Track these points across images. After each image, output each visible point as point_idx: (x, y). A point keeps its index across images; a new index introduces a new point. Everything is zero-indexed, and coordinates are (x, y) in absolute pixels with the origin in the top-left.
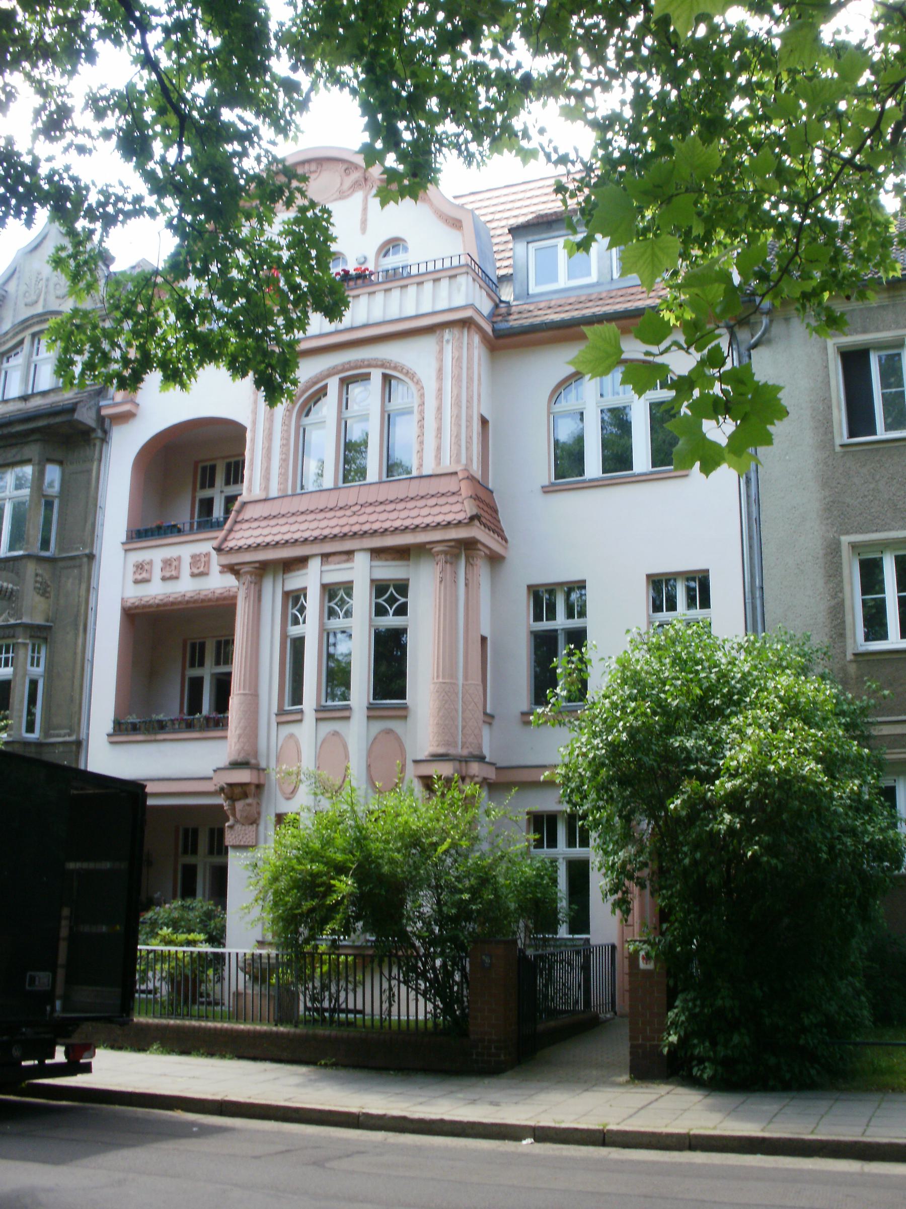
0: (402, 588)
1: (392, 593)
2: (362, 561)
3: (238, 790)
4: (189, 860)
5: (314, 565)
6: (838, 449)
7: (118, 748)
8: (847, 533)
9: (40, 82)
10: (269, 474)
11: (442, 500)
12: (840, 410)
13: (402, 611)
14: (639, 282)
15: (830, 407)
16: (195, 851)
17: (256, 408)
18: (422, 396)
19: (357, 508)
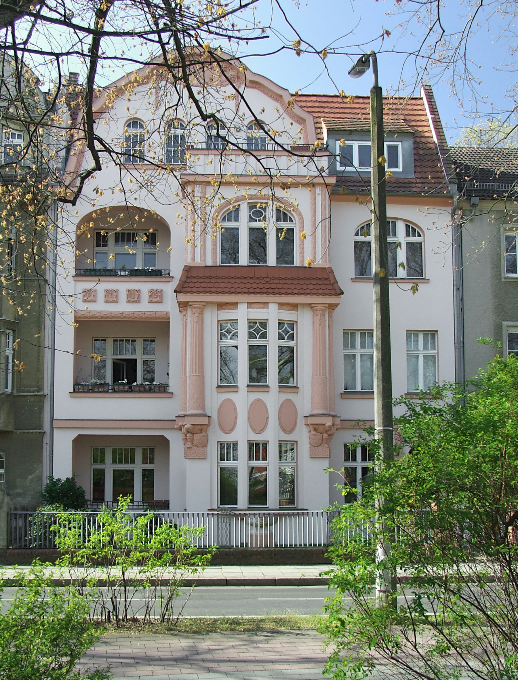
0: (292, 325)
1: (286, 328)
2: (273, 308)
3: (197, 428)
4: (99, 466)
5: (243, 308)
6: (503, 280)
7: (74, 399)
8: (505, 320)
9: (155, 25)
10: (205, 252)
11: (320, 282)
12: (504, 260)
13: (291, 337)
14: (6, 29)
15: (500, 259)
16: (102, 461)
17: (315, 242)
18: (303, 222)
19: (267, 280)
